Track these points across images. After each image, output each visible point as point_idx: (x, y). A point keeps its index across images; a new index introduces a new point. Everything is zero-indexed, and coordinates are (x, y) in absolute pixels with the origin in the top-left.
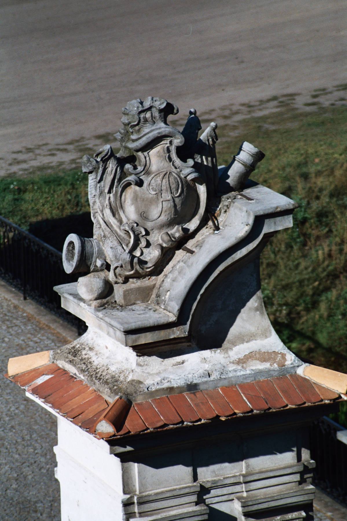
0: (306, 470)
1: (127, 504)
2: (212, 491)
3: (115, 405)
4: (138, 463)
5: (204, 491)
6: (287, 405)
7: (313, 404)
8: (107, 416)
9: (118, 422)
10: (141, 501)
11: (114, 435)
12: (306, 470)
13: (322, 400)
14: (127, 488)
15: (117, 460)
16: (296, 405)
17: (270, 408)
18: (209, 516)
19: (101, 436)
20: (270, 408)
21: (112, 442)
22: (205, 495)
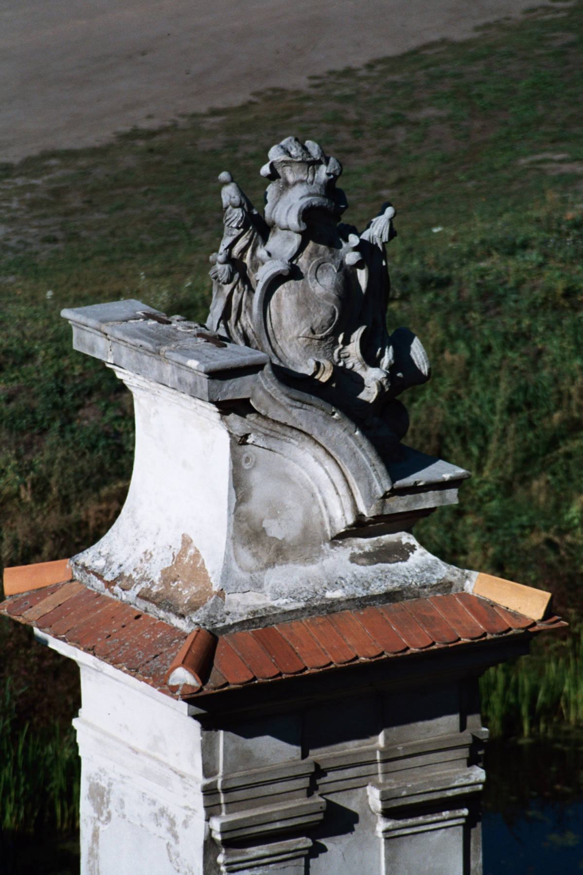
0: (476, 743)
1: (209, 792)
2: (329, 774)
3: (197, 639)
4: (226, 729)
5: (319, 772)
6: (459, 639)
7: (368, 660)
8: (187, 661)
9: (203, 667)
10: (229, 786)
11: (201, 690)
12: (476, 743)
13: (510, 629)
14: (208, 770)
15: (196, 725)
16: (497, 634)
17: (280, 674)
18: (324, 815)
19: (172, 691)
20: (255, 679)
21: (193, 699)
22: (320, 778)
